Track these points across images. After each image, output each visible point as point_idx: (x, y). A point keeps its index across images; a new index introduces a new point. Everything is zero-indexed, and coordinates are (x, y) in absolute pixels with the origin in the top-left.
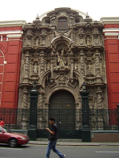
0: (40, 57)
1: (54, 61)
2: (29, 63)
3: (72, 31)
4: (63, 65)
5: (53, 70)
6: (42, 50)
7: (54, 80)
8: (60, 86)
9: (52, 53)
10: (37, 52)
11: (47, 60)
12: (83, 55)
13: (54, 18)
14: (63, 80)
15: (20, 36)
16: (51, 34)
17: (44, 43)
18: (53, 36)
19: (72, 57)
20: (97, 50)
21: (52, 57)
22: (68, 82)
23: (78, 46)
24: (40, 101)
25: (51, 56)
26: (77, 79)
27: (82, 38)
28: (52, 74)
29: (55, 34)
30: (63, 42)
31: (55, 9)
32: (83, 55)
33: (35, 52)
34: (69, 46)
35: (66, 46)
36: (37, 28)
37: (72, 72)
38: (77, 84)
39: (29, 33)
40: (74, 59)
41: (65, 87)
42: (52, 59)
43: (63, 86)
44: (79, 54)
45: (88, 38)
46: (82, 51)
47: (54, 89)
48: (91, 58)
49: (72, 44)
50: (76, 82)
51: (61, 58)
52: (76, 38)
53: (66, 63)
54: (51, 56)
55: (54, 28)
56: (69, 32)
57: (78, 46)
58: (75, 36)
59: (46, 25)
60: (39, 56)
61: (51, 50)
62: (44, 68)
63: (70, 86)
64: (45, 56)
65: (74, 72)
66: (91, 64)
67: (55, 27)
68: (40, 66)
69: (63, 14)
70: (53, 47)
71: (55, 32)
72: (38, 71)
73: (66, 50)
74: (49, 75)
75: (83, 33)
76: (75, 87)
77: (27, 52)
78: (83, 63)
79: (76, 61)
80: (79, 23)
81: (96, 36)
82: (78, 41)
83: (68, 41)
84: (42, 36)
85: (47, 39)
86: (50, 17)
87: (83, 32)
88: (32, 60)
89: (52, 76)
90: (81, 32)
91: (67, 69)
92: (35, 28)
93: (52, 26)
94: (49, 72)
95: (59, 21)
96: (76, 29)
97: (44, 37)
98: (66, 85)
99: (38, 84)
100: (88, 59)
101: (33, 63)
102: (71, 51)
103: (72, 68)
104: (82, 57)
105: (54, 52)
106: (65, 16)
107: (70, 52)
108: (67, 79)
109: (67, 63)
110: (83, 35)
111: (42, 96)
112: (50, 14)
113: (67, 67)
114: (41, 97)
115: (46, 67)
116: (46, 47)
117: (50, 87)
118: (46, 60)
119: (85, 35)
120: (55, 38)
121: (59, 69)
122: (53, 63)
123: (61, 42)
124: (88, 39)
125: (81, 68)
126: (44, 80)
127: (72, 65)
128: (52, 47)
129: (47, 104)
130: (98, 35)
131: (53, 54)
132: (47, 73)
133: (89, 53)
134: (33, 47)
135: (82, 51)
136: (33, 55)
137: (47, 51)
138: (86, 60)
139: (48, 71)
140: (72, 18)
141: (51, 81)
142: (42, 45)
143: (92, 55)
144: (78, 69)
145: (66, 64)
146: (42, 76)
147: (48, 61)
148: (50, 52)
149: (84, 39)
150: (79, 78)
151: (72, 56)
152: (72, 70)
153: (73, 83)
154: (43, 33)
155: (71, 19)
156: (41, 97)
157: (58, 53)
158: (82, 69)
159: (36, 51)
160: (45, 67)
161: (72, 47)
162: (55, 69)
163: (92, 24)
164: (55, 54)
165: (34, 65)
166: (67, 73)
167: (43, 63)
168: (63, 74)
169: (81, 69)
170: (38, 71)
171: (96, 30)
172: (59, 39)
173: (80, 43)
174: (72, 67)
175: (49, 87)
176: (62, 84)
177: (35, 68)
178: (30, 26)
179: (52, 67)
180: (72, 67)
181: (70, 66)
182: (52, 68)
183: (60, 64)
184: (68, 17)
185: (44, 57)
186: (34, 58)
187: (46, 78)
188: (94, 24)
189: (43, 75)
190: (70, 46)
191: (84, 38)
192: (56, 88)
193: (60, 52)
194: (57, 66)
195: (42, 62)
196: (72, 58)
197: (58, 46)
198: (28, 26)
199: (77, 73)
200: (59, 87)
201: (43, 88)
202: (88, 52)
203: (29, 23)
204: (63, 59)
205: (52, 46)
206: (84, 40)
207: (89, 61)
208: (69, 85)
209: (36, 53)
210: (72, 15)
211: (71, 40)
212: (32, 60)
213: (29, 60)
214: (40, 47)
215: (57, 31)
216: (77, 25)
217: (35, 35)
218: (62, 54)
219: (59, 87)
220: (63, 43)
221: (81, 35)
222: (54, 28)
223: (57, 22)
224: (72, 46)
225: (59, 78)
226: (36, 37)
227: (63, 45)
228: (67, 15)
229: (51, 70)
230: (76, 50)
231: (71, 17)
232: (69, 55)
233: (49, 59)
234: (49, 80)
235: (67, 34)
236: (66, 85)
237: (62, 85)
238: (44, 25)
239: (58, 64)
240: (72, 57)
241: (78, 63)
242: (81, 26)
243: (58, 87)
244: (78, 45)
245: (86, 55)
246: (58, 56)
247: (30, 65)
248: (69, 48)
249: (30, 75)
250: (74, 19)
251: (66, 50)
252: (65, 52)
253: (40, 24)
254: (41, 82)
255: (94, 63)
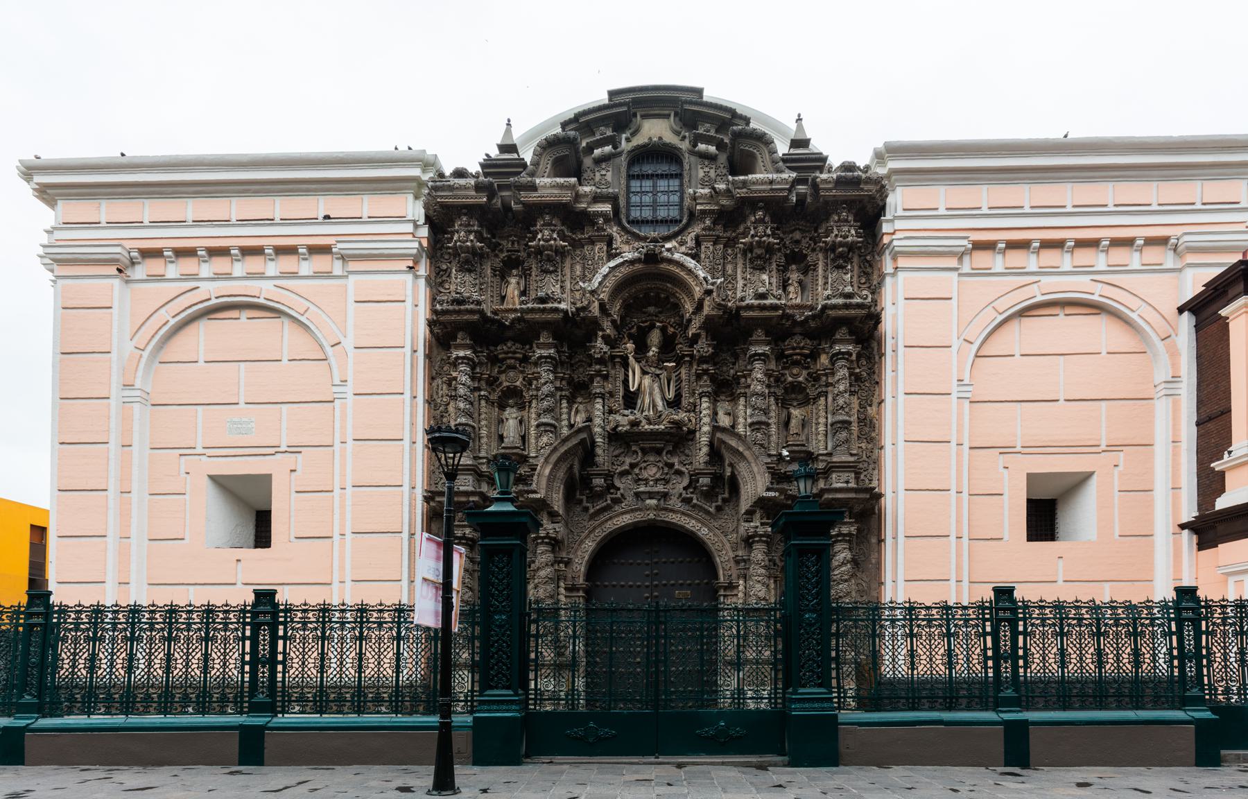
0: (536, 364)
1: (609, 387)
2: (476, 394)
3: (709, 229)
4: (660, 405)
5: (603, 428)
6: (546, 325)
7: (609, 476)
8: (640, 505)
9: (599, 343)
10: (515, 340)
11: (570, 382)
12: (763, 357)
13: (608, 149)
14: (657, 481)
15: (415, 251)
16: (592, 242)
17: (551, 286)
18: (604, 255)
19: (705, 366)
20: (844, 330)
21: (598, 367)
22: (685, 488)
23: (744, 304)
24: (542, 573)
25: (592, 360)
26: (733, 473)
27: (762, 269)
28: (599, 451)
29: (610, 241)
30: (659, 284)
31: (612, 94)
32: (763, 357)
33: (504, 341)
34: (689, 307)
35: (677, 307)
36: (507, 208)
37: (705, 439)
38: (726, 495)
39: (463, 236)
40: (713, 379)
41: (666, 509)
42: (598, 373)
43: (657, 508)
44: (745, 351)
45: (794, 267)
46: (759, 334)
47: (611, 518)
48: (805, 373)
49: (709, 292)
50: (721, 486)
51: (644, 373)
52: (729, 268)
53: (671, 395)
54: (592, 360)
55: (606, 208)
56: (693, 234)
57: (739, 308)
58: (724, 258)
59: (561, 186)
60: (525, 360)
61: (594, 325)
62: (558, 420)
63: (694, 506)
64: (562, 363)
65: (719, 435)
66: (806, 401)
67: (613, 199)
68: (533, 410)
69: (656, 130)
70: (602, 306)
71: (614, 230)
72: (523, 438)
73: (671, 330)
74: (586, 451)
75: (771, 240)
76: (719, 509)
77: (460, 335)
78: (762, 395)
79: (725, 388)
80: (750, 176)
81: (841, 256)
82: (740, 283)
83: (690, 280)
84: (539, 251)
85: (567, 271)
86: (584, 144)
87: (769, 232)
88: (492, 382)
89: (602, 454)
90: (757, 230)
91: (678, 424)
92: (497, 202)
93: (597, 199)
94: (584, 435)
95: (636, 170)
96: (730, 217)
97: (550, 259)
98: (675, 502)
99: (531, 496)
100: (790, 379)
101: (494, 397)
102: (703, 334)
103: (706, 420)
104: (758, 365)
105: (606, 339)
106: (670, 138)
107: (696, 338)
108: (679, 473)
109: (678, 396)
110: (769, 249)
111: (553, 551)
112: (584, 122)
113: (682, 416)
114: (549, 557)
115: (569, 414)
116: (565, 312)
117: (592, 511)
118: (569, 384)
119: (779, 250)
120: (612, 264)
121: (634, 424)
122: (602, 396)
123: (650, 289)
124: (794, 276)
125: (749, 421)
126: (561, 474)
127: (705, 405)
128: (595, 309)
129: (578, 590)
130: (851, 247)
131: (606, 348)
132: (574, 441)
133: (794, 349)
134: (495, 312)
135: (759, 334)
136: (496, 356)
137: (573, 332)
138: (777, 380)
139: (580, 430)
140: (712, 149)
141: (598, 482)
142: (542, 300)
143: (814, 356)
144: (733, 427)
145: (675, 404)
146: (549, 455)
147: (578, 390)
148: (591, 336)
149: (774, 273)
150: (742, 468)
151: (702, 360)
152: (706, 429)
153: (709, 495)
154: (546, 235)
155: (704, 156)
156: (549, 557)
157: (630, 346)
158: (756, 426)
159: (509, 333)
160: (565, 416)
161: (706, 310)
162: (617, 426)
163: (825, 181)
164: (617, 352)
165: (502, 407)
166: (676, 447)
167: (551, 395)
168: (658, 452)
169: (751, 425)
170: (523, 438)
171: (846, 221)
172: (638, 266)
173: (752, 287)
174: (705, 417)
175: (586, 509)
176: (651, 495)
177: (511, 421)
178: (465, 188)
179: (599, 417)
180: (705, 417)
181: (693, 408)
182: (598, 421)
183: (639, 401)
184: (685, 146)
185: (555, 367)
186: (500, 372)
187: (571, 467)
188: (840, 182)
189: (555, 449)
190: (699, 307)
191: (774, 266)
192: (623, 513)
193: (642, 348)
194: (626, 412)
195: (545, 389)
196: (706, 372)
197: (628, 308)
198: (451, 188)
199: (733, 442)
200: (636, 510)
201: (553, 515)
202: (796, 341)
203: (460, 173)
204: (658, 375)
205: (596, 304)
206: (774, 280)
207: (796, 388)
208: (687, 501)
209: (509, 344)
210: (712, 133)
211: (701, 274)
212: (492, 382)
213: (473, 378)
214: (532, 310)
215: (624, 228)
216: (742, 193)
217: (501, 251)
218: (651, 353)
219: (636, 510)
220: (658, 295)
221: (758, 251)
222: (606, 208)
223: (624, 174)
224: (706, 303)
225: (637, 470)
226: (503, 261)
227: (657, 302)
228: (677, 133)
229: (597, 430)
230: (731, 330)
231: (702, 147)
232: (692, 356)
233: (580, 375)
234: (586, 481)
235: (682, 243)
236: (675, 502)
237: (654, 502)
238: (548, 185)
239: (631, 400)
240: (705, 366)
241: (734, 399)
242: (761, 199)
243: (632, 511)
244: (742, 299)
245: (780, 356)
246: (632, 360)
247: (483, 402)
248: (690, 321)
249: (483, 454)
250: (723, 158)
251: (671, 330)
252: (667, 346)
253: (524, 178)
254: (545, 483)
255: (819, 396)
